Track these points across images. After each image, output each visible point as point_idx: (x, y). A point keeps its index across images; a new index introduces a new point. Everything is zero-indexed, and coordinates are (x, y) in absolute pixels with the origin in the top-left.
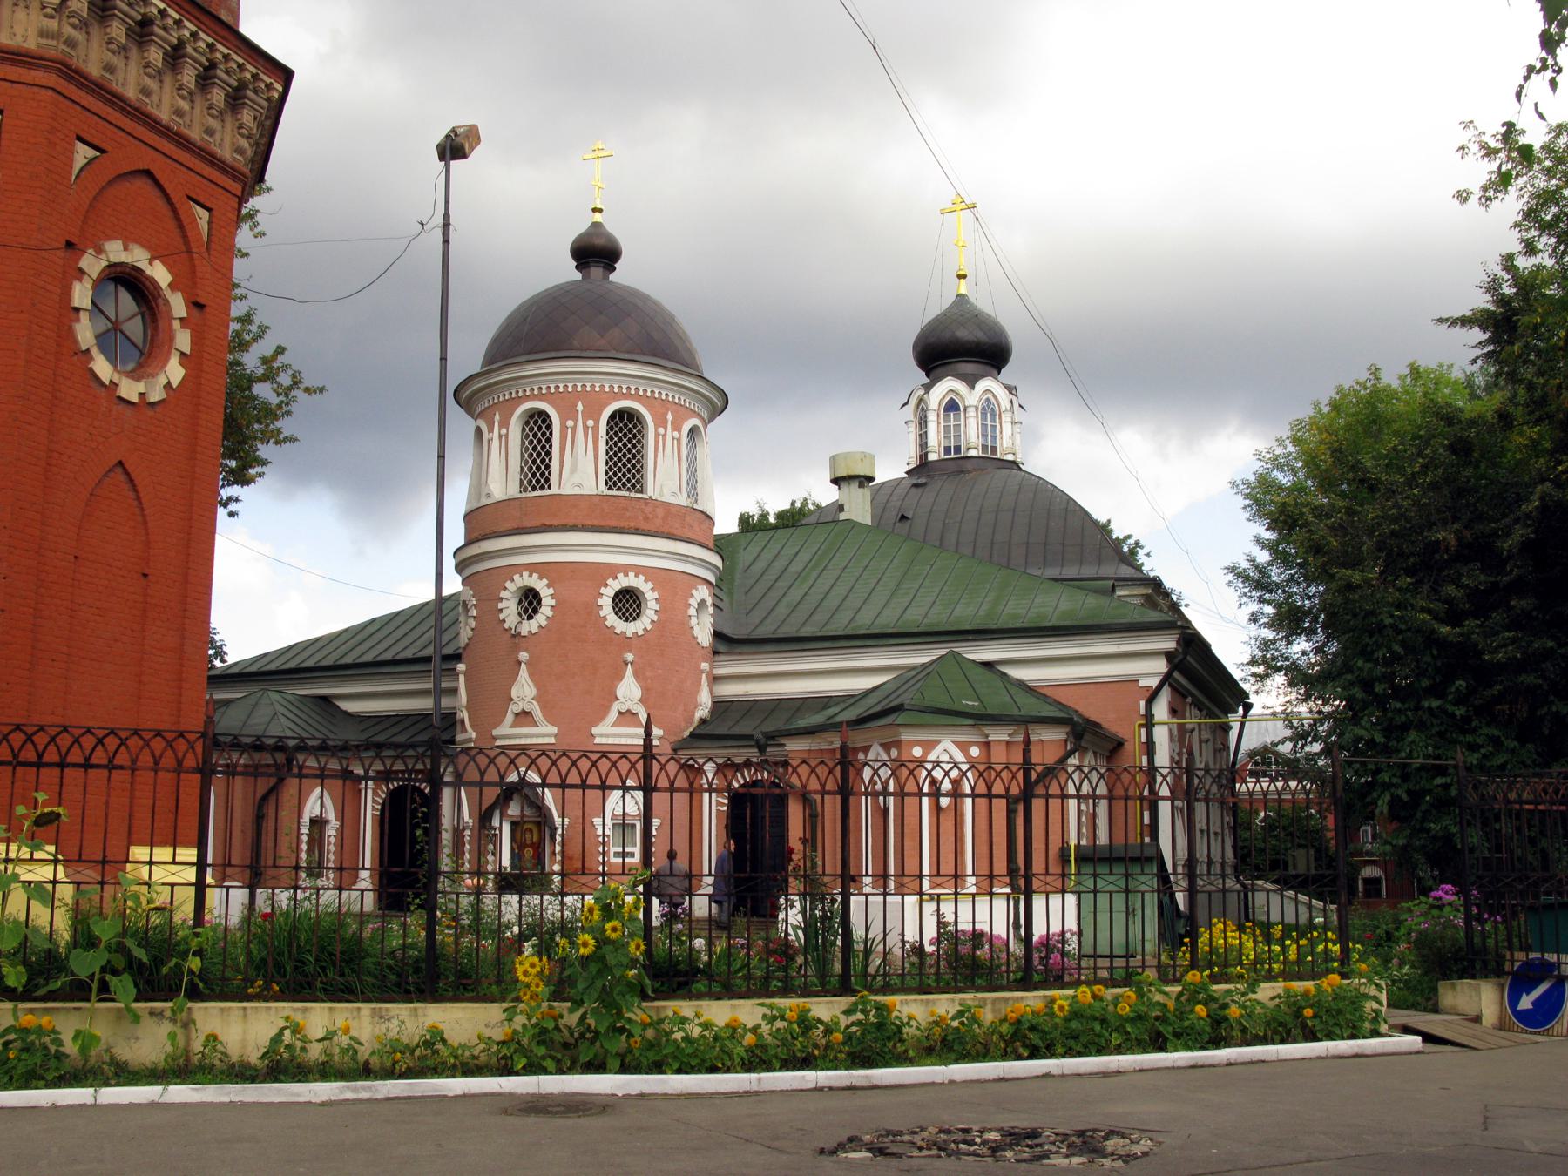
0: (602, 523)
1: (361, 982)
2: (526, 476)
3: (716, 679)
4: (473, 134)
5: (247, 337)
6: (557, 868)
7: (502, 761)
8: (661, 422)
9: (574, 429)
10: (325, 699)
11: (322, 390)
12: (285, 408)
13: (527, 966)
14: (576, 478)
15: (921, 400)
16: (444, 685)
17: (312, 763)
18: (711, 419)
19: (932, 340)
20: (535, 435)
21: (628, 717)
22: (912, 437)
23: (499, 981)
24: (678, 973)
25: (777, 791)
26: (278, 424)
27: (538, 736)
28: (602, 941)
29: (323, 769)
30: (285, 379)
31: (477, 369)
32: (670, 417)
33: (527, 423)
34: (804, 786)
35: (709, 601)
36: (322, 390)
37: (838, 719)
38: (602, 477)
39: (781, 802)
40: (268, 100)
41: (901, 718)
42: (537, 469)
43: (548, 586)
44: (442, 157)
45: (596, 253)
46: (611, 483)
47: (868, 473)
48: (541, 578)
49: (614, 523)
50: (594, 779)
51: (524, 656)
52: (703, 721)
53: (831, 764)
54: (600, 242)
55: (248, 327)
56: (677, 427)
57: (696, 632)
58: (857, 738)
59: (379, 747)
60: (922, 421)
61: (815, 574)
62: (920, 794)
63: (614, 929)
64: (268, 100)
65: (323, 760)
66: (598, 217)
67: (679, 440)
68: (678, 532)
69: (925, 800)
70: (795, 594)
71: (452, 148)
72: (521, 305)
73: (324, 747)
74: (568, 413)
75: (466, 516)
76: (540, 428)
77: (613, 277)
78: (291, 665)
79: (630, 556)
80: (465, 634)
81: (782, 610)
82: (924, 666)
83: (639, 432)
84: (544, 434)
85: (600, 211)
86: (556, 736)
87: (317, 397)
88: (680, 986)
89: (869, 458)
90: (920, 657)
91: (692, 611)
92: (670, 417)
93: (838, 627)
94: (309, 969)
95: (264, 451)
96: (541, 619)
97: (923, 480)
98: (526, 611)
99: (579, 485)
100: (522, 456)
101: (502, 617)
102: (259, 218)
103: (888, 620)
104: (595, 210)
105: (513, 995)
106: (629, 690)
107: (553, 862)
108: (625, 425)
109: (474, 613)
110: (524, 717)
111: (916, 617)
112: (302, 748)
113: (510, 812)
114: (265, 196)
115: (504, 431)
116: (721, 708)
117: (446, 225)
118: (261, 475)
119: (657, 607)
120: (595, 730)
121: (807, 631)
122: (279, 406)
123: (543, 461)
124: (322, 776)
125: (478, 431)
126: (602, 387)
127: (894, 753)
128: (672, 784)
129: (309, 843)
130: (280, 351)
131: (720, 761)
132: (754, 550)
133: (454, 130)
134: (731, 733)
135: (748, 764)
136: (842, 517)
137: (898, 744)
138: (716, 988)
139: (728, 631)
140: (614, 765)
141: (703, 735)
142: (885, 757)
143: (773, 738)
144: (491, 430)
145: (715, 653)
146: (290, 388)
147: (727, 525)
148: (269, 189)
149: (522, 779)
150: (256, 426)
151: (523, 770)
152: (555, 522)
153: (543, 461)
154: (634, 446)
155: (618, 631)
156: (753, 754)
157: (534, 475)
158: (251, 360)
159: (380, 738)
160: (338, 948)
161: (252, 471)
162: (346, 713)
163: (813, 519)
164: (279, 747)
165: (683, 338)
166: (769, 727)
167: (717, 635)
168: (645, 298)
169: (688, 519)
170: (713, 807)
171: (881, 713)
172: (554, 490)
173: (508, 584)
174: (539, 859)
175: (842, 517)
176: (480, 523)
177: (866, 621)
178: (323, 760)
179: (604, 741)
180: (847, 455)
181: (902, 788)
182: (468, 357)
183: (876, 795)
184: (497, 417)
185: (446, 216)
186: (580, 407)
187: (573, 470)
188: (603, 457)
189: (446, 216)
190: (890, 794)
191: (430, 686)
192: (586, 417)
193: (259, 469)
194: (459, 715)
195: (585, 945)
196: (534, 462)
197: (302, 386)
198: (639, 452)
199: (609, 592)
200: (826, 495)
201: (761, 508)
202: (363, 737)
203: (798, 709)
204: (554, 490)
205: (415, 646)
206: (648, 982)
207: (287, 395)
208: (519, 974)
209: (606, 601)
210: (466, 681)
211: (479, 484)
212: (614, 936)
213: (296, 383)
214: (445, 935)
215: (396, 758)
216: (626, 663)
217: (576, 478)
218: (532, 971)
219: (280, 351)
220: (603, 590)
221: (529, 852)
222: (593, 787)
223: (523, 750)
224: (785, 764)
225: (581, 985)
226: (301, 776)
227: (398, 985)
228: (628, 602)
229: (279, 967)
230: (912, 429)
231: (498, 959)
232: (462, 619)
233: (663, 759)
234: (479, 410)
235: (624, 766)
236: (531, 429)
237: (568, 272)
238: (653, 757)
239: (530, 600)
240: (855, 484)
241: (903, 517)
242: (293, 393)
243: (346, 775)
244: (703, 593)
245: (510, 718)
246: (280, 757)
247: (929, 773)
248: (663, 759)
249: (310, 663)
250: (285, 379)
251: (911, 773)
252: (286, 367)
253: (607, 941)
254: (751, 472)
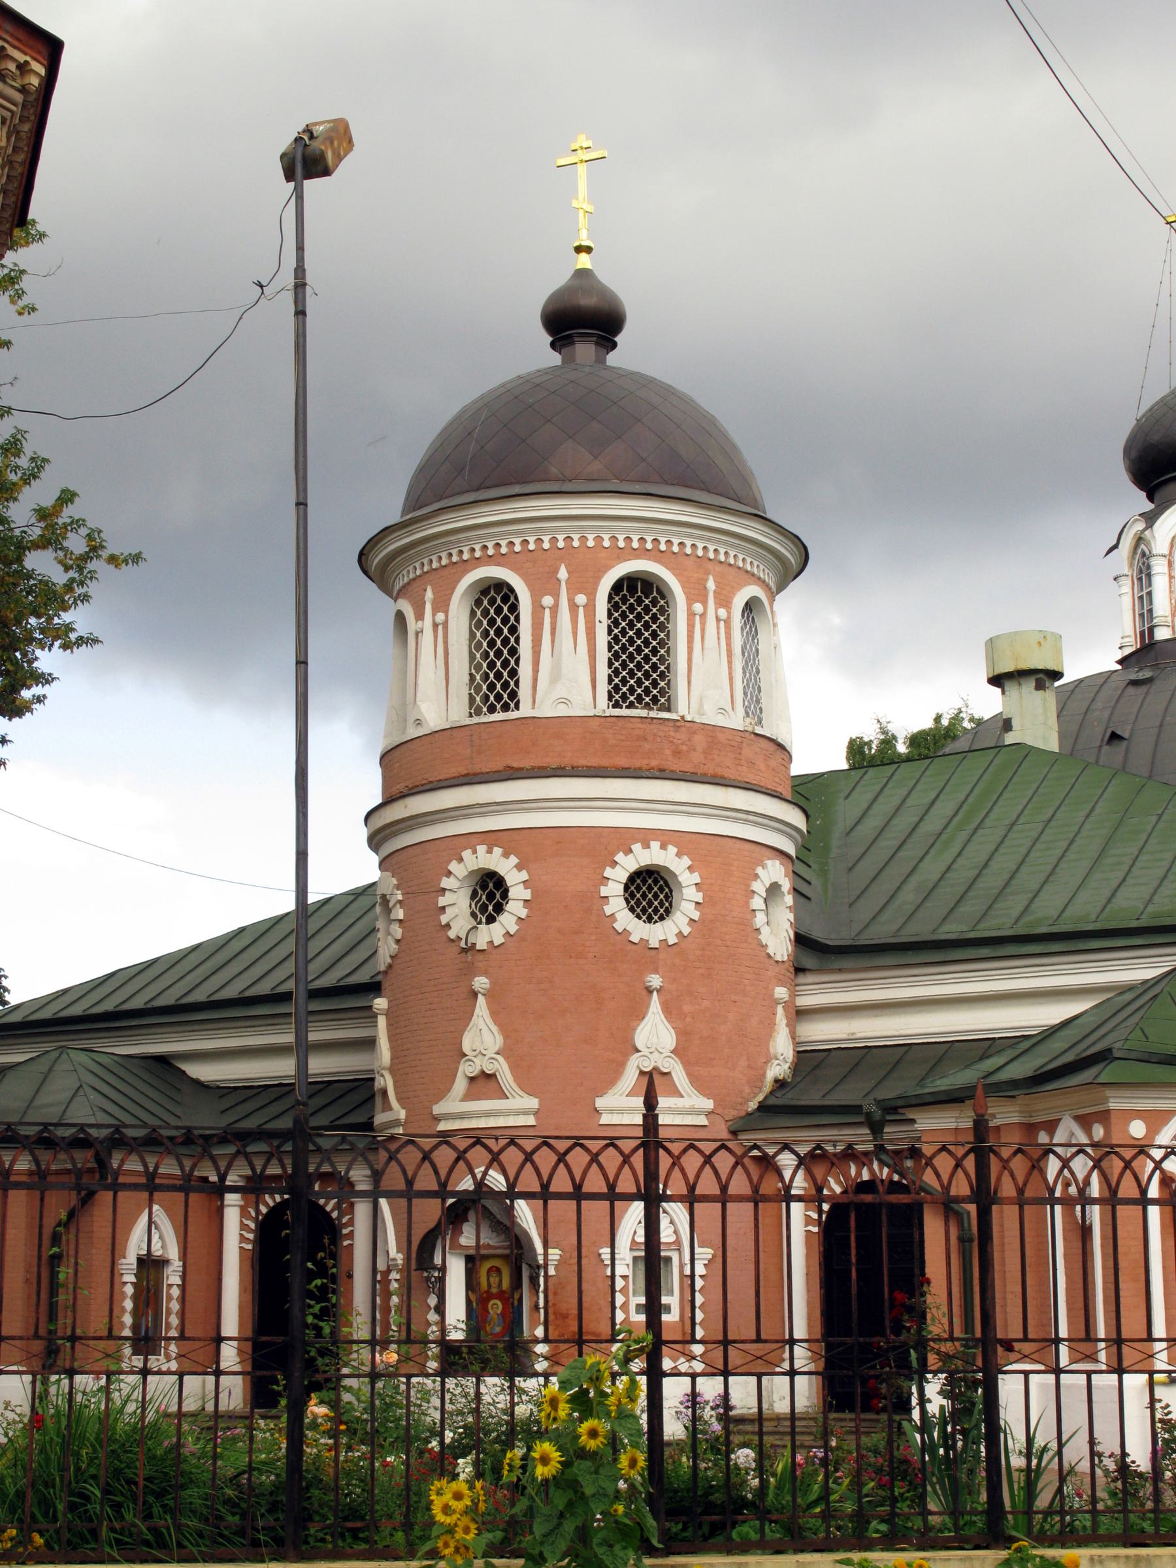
0: (604, 762)
1: (178, 1527)
2: (478, 689)
3: (800, 1014)
4: (341, 135)
5: (13, 477)
6: (540, 1332)
7: (444, 1157)
8: (697, 593)
9: (555, 610)
10: (163, 1061)
11: (136, 558)
12: (79, 591)
13: (447, 1497)
14: (560, 691)
15: (1139, 540)
16: (313, 1037)
17: (133, 1164)
18: (782, 586)
19: (1155, 438)
20: (492, 622)
21: (481, 1083)
22: (1127, 602)
23: (408, 1526)
24: (710, 1508)
25: (903, 1199)
26: (66, 617)
27: (488, 1114)
28: (575, 1454)
29: (152, 1176)
30: (76, 543)
31: (395, 517)
32: (711, 585)
33: (478, 603)
34: (946, 1188)
35: (786, 885)
36: (136, 558)
37: (1003, 1076)
38: (603, 687)
39: (908, 1220)
40: (23, 90)
41: (1107, 1073)
42: (497, 678)
43: (519, 867)
44: (289, 175)
45: (583, 320)
46: (617, 696)
47: (1051, 666)
48: (506, 855)
49: (622, 762)
50: (561, 1183)
51: (481, 983)
52: (780, 1084)
53: (960, 1152)
54: (588, 301)
55: (15, 461)
56: (724, 601)
57: (765, 936)
58: (1041, 1105)
59: (244, 1137)
60: (1144, 575)
61: (963, 836)
62: (1144, 1201)
63: (593, 1434)
64: (23, 90)
65: (188, 1164)
66: (584, 261)
67: (728, 622)
68: (730, 774)
69: (1154, 1212)
70: (931, 870)
71: (305, 159)
72: (464, 411)
73: (152, 1142)
74: (544, 584)
75: (383, 757)
76: (499, 611)
77: (613, 359)
78: (108, 1006)
79: (651, 814)
80: (386, 949)
81: (909, 896)
82: (1147, 985)
83: (662, 611)
84: (505, 620)
85: (588, 250)
86: (536, 1113)
87: (127, 570)
88: (717, 1529)
89: (1051, 640)
90: (1138, 969)
91: (757, 903)
92: (711, 585)
93: (1000, 923)
94: (94, 1508)
95: (46, 660)
96: (507, 922)
97: (1146, 674)
98: (484, 909)
99: (565, 701)
100: (472, 657)
101: (444, 919)
102: (25, 283)
103: (1086, 910)
104: (579, 249)
105: (427, 1546)
106: (655, 1036)
107: (533, 1327)
108: (638, 600)
109: (400, 913)
110: (484, 1083)
111: (1131, 905)
112: (118, 1140)
113: (463, 1241)
114: (34, 246)
115: (440, 617)
116: (809, 1061)
117: (300, 286)
118: (40, 699)
119: (699, 897)
120: (600, 1103)
121: (950, 930)
122: (69, 587)
123: (505, 664)
124: (151, 1186)
125: (400, 617)
126: (599, 539)
127: (1099, 1132)
128: (724, 1188)
129: (136, 1298)
130: (67, 497)
131: (803, 1150)
132: (862, 797)
133: (308, 130)
134: (827, 1102)
135: (850, 1154)
136: (1010, 739)
137: (1104, 1117)
138: (772, 1532)
139: (818, 933)
140: (595, 1158)
141: (780, 1108)
142: (1084, 1139)
143: (894, 1110)
144: (420, 616)
145: (799, 970)
146: (85, 558)
147: (818, 752)
148: (42, 236)
149: (480, 1184)
150: (33, 621)
151: (479, 1171)
152: (527, 763)
153: (505, 664)
154: (654, 635)
155: (635, 938)
156: (861, 1138)
157: (491, 687)
158: (21, 514)
159: (251, 1124)
160: (142, 1471)
161: (26, 694)
162: (197, 1083)
163: (962, 744)
164: (81, 1142)
165: (729, 450)
166: (888, 1092)
167: (801, 940)
168: (666, 391)
169: (747, 752)
170: (800, 1221)
171: (1071, 1066)
172: (525, 710)
173: (453, 866)
174: (513, 1319)
175: (1010, 739)
176: (409, 768)
177: (1048, 912)
178: (151, 1161)
179: (616, 1119)
180: (1013, 636)
181: (1113, 1191)
182: (368, 495)
183: (1067, 1202)
184: (429, 594)
185: (300, 271)
186: (563, 574)
187: (555, 677)
188: (603, 655)
189: (300, 271)
190: (1094, 1201)
191: (289, 1038)
192: (573, 591)
193: (37, 690)
194: (379, 1083)
195: (545, 1460)
196: (491, 665)
197: (105, 554)
198: (662, 644)
199: (618, 875)
200: (988, 703)
201: (884, 731)
202: (224, 1121)
203: (940, 1060)
204: (525, 710)
205: (306, 970)
206: (651, 1522)
207: (81, 569)
208: (436, 1510)
209: (614, 889)
210: (389, 1025)
211: (404, 704)
212: (592, 1444)
213: (95, 549)
214: (317, 1446)
215: (269, 1156)
216: (650, 991)
217: (560, 691)
218: (458, 1505)
219: (67, 497)
220: (608, 872)
221: (496, 1307)
222: (560, 1196)
223: (478, 1139)
224: (914, 1153)
225: (539, 1529)
226: (116, 1187)
227: (241, 1532)
228: (650, 891)
229: (46, 1505)
230: (1126, 587)
231: (408, 1487)
232: (380, 924)
233: (676, 1148)
234: (399, 584)
235: (611, 1160)
236: (486, 613)
237: (538, 353)
238: (659, 1145)
239: (490, 892)
240: (1029, 685)
241: (1115, 737)
242: (91, 566)
243: (188, 1185)
244: (774, 872)
245: (460, 1085)
246: (83, 1158)
247: (1158, 1165)
248: (676, 1148)
249: (137, 1003)
250: (76, 543)
251: (1128, 1165)
252: (77, 523)
253: (582, 1454)
254: (843, 672)
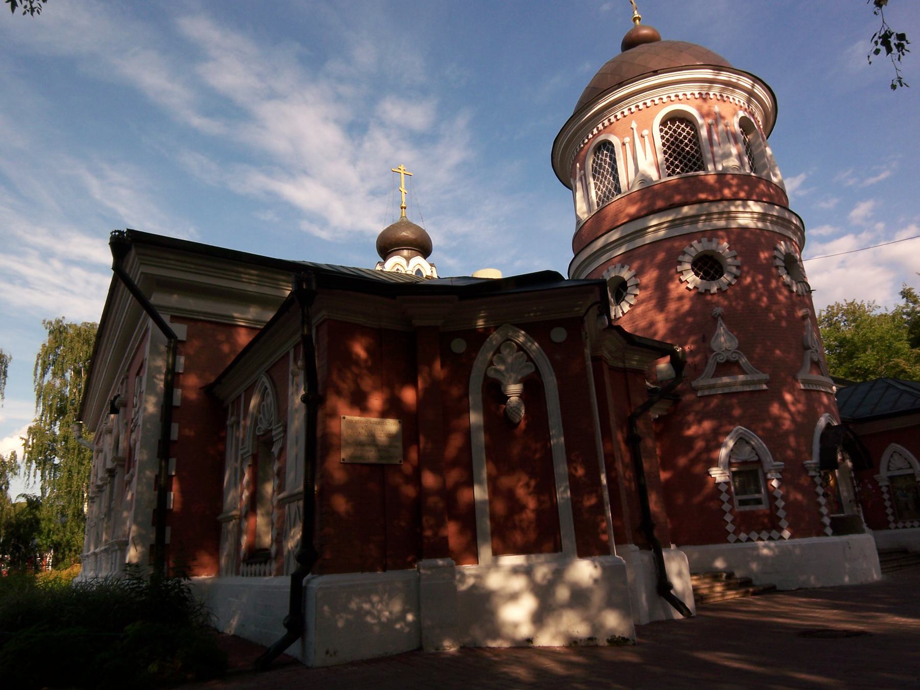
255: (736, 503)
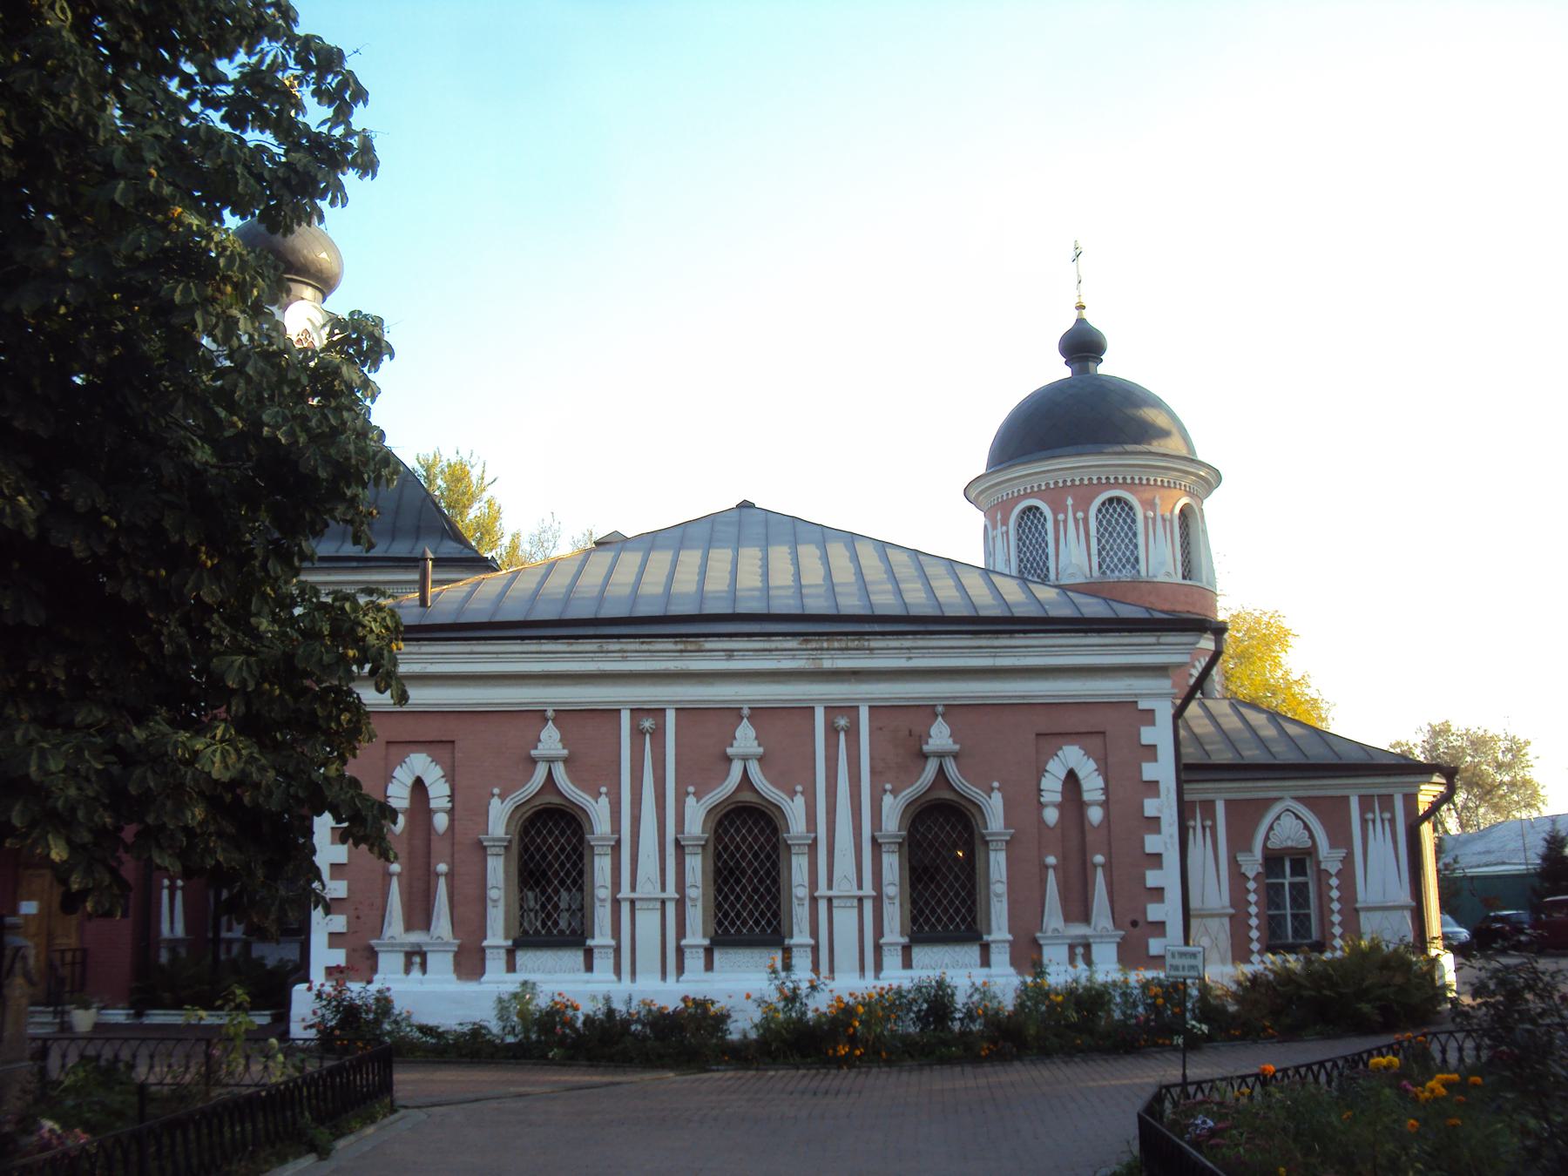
9: (1065, 521)
45: (1082, 346)
186: (1070, 502)
255: (1200, 957)
